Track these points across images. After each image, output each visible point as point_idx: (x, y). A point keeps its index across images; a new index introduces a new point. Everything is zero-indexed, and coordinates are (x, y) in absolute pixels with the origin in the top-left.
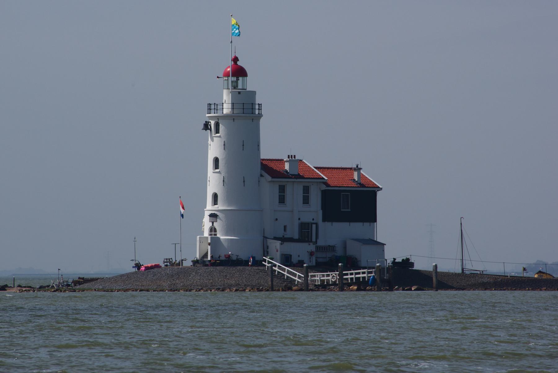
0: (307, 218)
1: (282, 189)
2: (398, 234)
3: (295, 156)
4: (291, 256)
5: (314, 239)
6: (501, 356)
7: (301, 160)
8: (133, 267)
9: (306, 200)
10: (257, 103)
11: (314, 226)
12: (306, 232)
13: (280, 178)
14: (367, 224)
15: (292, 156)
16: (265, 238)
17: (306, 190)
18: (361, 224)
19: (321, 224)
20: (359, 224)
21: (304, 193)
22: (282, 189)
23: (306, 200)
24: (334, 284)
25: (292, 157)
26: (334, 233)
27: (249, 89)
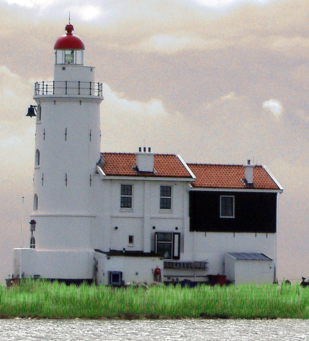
0: (166, 226)
1: (127, 190)
3: (149, 149)
4: (121, 273)
5: (176, 254)
7: (173, 156)
9: (166, 204)
10: (96, 81)
11: (176, 236)
12: (164, 246)
14: (261, 236)
15: (145, 148)
17: (166, 191)
18: (231, 235)
22: (127, 190)
23: (166, 204)
25: (145, 150)
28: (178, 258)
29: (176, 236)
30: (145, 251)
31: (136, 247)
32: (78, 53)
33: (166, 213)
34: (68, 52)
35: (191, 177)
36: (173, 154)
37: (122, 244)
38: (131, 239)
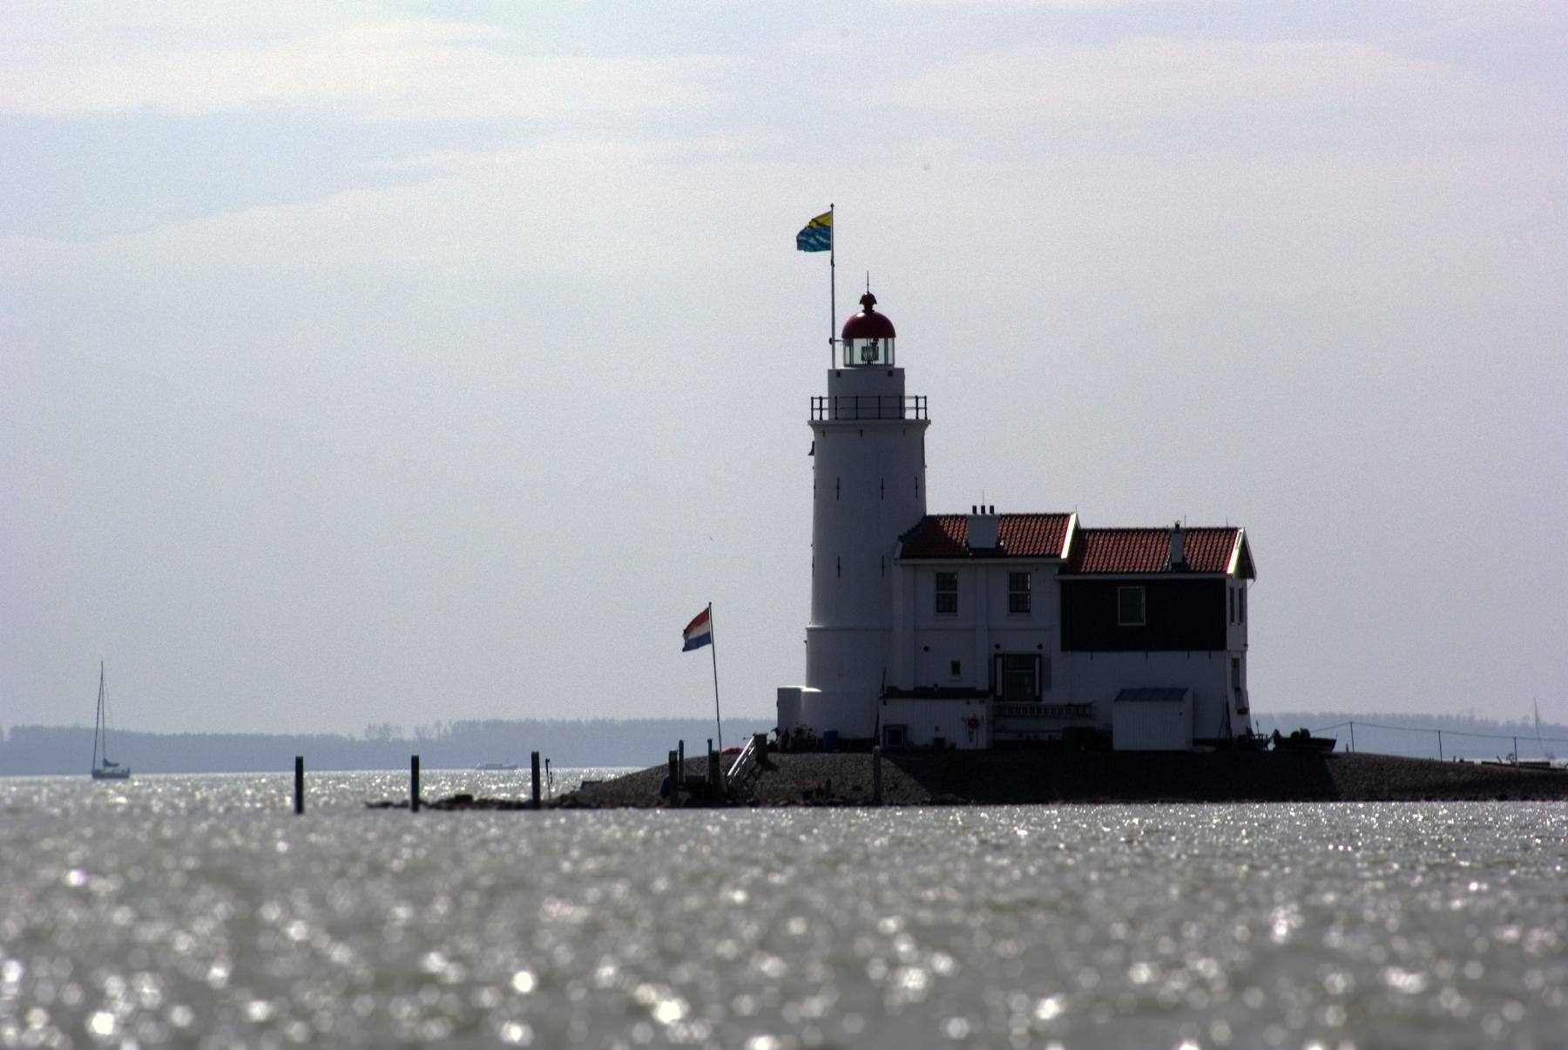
2: (1286, 679)
6: (349, 813)
9: (1019, 604)
12: (1018, 676)
13: (941, 557)
14: (1199, 658)
15: (983, 508)
17: (1018, 582)
20: (1179, 656)
23: (1019, 604)
26: (1086, 679)
28: (1039, 698)
30: (979, 688)
31: (965, 681)
37: (945, 679)
38: (956, 667)
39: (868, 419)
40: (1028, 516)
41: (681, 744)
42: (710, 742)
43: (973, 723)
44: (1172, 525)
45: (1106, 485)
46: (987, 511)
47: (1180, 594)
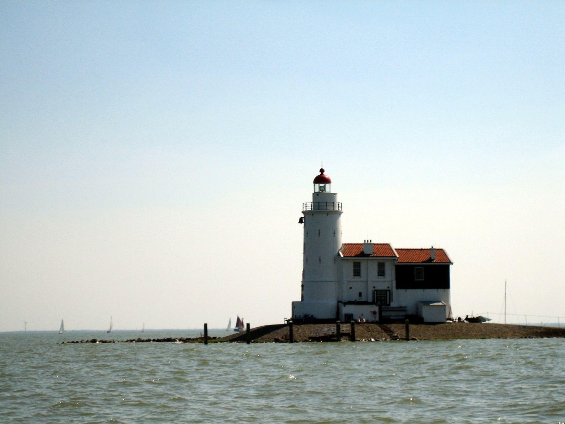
2: (463, 299)
5: (388, 303)
7: (442, 249)
8: (248, 325)
9: (381, 273)
11: (388, 292)
12: (381, 298)
16: (339, 302)
18: (422, 290)
19: (395, 292)
21: (384, 270)
23: (381, 273)
24: (333, 336)
26: (406, 298)
27: (332, 192)
28: (389, 305)
29: (388, 292)
31: (363, 299)
32: (327, 185)
33: (381, 279)
34: (322, 185)
35: (396, 256)
36: (441, 248)
37: (355, 297)
38: (360, 294)
39: (321, 214)
40: (354, 244)
41: (206, 325)
42: (230, 322)
43: (374, 313)
44: (430, 247)
45: (405, 235)
46: (369, 242)
47: (430, 271)
